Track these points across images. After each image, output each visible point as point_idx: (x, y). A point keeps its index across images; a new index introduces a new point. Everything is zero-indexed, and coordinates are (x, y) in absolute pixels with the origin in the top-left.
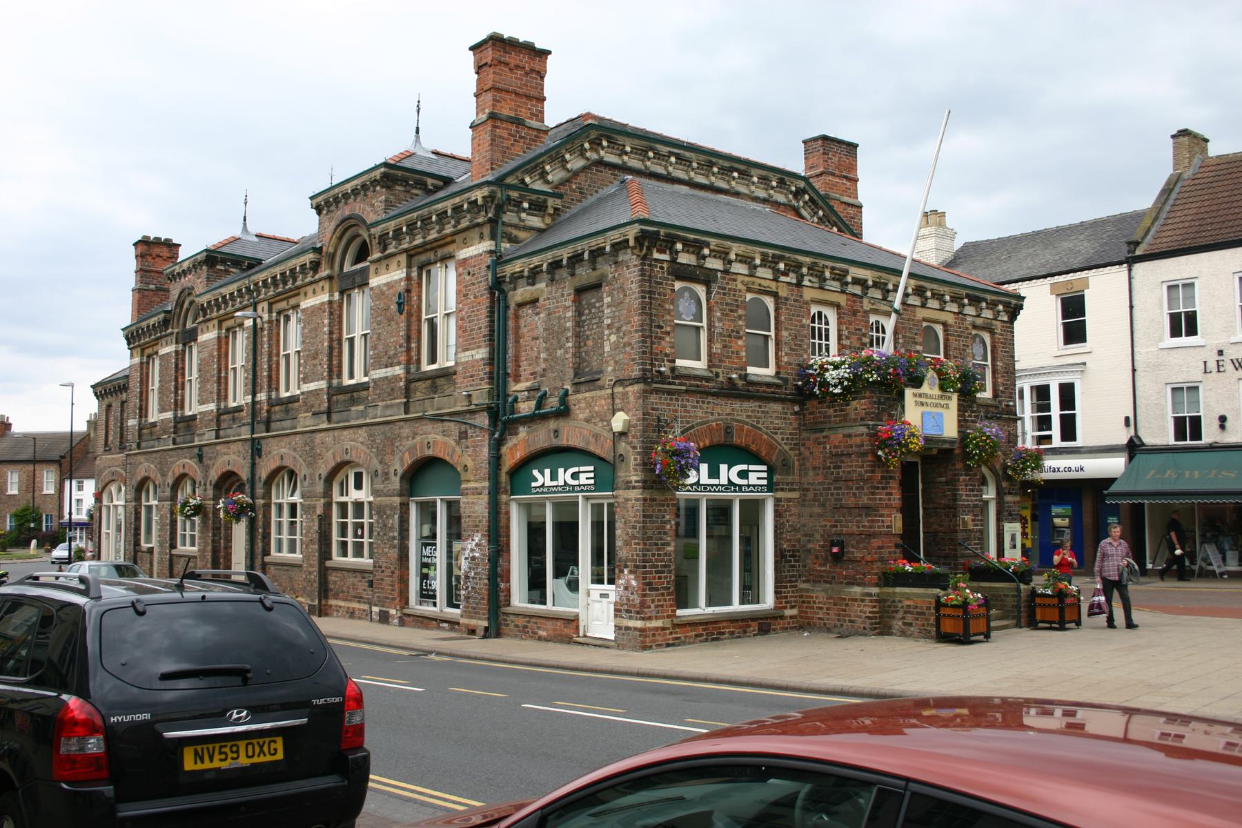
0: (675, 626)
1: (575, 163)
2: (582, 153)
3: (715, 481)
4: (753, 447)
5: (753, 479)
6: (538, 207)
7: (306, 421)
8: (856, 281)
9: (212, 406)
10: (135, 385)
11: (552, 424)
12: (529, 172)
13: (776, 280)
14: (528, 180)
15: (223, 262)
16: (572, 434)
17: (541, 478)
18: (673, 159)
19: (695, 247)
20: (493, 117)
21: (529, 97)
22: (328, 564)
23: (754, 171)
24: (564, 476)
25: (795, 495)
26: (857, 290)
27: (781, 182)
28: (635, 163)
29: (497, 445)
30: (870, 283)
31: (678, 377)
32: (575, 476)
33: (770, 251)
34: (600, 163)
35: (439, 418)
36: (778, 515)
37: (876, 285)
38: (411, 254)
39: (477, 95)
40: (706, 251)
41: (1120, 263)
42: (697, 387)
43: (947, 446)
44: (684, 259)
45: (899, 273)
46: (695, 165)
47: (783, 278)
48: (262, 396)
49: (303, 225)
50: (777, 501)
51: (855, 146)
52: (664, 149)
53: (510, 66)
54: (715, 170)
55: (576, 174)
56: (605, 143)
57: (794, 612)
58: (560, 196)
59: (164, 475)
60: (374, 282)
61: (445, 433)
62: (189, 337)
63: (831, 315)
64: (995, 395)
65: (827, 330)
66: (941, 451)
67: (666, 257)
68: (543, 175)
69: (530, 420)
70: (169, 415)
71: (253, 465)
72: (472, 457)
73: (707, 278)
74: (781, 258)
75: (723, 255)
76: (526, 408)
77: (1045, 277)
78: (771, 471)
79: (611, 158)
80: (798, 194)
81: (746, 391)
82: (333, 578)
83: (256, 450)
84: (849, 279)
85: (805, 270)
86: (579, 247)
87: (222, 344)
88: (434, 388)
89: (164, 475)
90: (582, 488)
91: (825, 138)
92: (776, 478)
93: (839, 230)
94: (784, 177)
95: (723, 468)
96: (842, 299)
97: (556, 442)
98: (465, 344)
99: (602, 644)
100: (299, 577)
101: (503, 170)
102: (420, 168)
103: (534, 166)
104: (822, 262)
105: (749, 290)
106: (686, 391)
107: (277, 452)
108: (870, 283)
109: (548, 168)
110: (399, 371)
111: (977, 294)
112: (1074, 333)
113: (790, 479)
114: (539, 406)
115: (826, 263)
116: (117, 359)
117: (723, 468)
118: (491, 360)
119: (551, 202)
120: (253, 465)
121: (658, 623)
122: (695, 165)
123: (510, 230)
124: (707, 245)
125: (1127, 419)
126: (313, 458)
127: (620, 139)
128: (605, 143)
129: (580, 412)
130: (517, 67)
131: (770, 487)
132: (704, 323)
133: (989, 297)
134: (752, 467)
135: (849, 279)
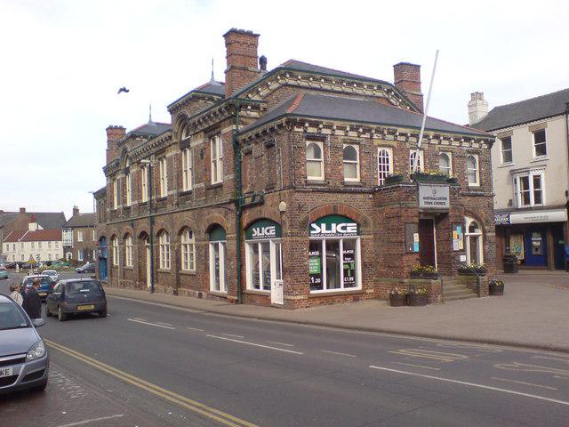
0: (310, 298)
1: (274, 86)
2: (277, 80)
3: (329, 232)
4: (348, 215)
5: (349, 230)
6: (256, 108)
7: (170, 208)
8: (401, 134)
9: (136, 202)
10: (108, 192)
11: (258, 208)
12: (250, 92)
13: (359, 137)
14: (250, 95)
15: (139, 137)
16: (265, 212)
17: (256, 232)
18: (323, 80)
19: (313, 124)
20: (232, 68)
21: (251, 57)
22: (180, 272)
23: (364, 83)
24: (264, 230)
25: (371, 237)
26: (403, 139)
27: (379, 88)
28: (303, 83)
29: (240, 216)
30: (409, 135)
31: (309, 185)
32: (268, 231)
33: (355, 124)
34: (287, 85)
35: (218, 206)
36: (362, 246)
37: (412, 135)
38: (206, 131)
39: (227, 57)
40: (321, 126)
41: (562, 114)
42: (317, 189)
43: (444, 211)
44: (311, 130)
45: (420, 128)
46: (334, 82)
47: (362, 136)
48: (154, 197)
49: (166, 118)
50: (362, 240)
51: (419, 66)
52: (318, 76)
53: (240, 43)
54: (249, 107)
55: (274, 91)
56: (288, 76)
57: (372, 291)
58: (266, 102)
59: (173, 228)
60: (193, 144)
61: (220, 213)
62: (127, 171)
63: (390, 151)
64: (481, 185)
65: (387, 159)
66: (441, 214)
67: (301, 130)
68: (258, 92)
69: (251, 206)
70: (121, 206)
71: (152, 228)
72: (229, 224)
73: (323, 139)
74: (361, 126)
75: (330, 127)
76: (248, 201)
77: (526, 123)
78: (358, 225)
79: (292, 82)
80: (389, 91)
81: (348, 190)
82: (182, 278)
83: (152, 223)
84: (397, 134)
85: (373, 131)
86: (265, 127)
87: (139, 173)
88: (216, 193)
89: (173, 228)
90: (271, 237)
91: (402, 64)
92: (361, 229)
93: (411, 109)
94: (380, 84)
95: (333, 225)
96: (395, 144)
97: (260, 216)
98: (225, 173)
99: (276, 307)
100: (170, 277)
101: (238, 92)
102: (211, 91)
103: (253, 89)
104: (382, 127)
105: (345, 143)
106: (313, 191)
107: (161, 222)
108: (409, 135)
109: (260, 89)
110: (202, 185)
111: (470, 136)
112: (541, 150)
113: (368, 229)
114: (253, 199)
115: (373, 126)
116: (101, 182)
117: (333, 225)
118: (235, 180)
119: (262, 105)
120: (152, 228)
121: (302, 297)
122: (334, 82)
123: (242, 119)
124: (321, 123)
125: (511, 201)
126: (173, 225)
127: (296, 73)
128: (288, 76)
129: (268, 202)
130: (244, 43)
131: (358, 234)
132: (322, 159)
133: (475, 137)
134: (349, 224)
135: (397, 134)
